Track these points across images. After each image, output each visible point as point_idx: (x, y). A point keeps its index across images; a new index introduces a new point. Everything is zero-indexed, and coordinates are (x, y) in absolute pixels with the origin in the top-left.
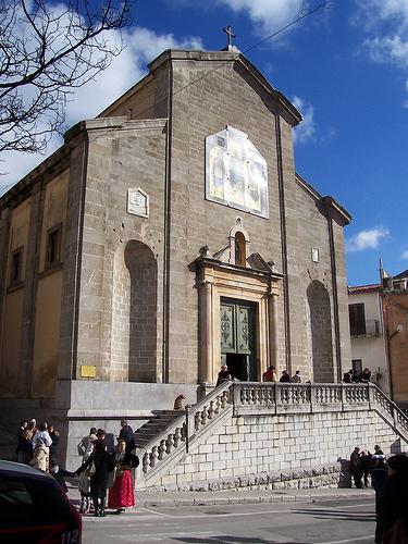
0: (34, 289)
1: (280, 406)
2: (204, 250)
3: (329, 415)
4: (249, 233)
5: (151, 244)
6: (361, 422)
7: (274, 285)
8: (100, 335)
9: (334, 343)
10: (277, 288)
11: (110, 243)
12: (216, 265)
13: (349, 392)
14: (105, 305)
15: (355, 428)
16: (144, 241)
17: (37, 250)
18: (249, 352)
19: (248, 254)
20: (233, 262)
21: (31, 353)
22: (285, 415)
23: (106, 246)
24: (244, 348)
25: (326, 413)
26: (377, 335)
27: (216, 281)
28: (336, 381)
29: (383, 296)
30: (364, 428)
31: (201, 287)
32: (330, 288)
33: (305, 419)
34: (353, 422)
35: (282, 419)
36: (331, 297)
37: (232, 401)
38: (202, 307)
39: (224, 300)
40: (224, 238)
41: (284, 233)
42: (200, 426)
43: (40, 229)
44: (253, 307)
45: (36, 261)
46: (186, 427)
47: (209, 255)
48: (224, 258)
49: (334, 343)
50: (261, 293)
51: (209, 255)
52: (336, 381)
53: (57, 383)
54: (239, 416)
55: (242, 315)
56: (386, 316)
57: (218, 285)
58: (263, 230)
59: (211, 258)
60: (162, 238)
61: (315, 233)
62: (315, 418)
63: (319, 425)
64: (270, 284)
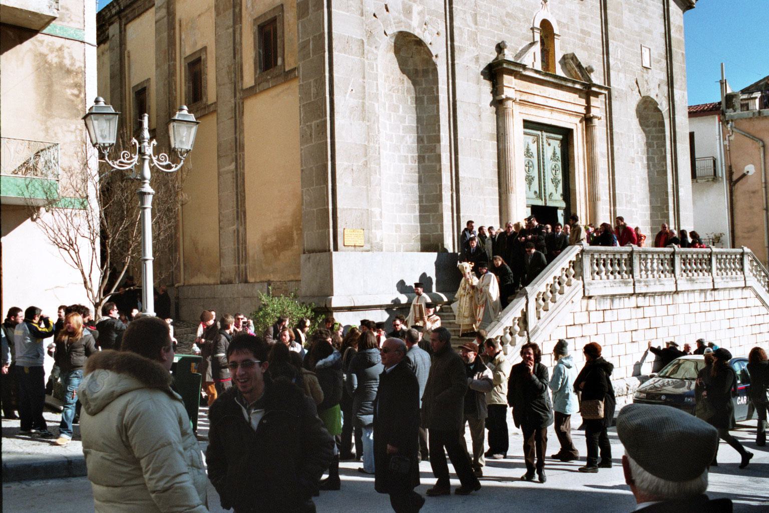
0: (238, 113)
1: (640, 282)
2: (500, 48)
3: (697, 294)
4: (559, 23)
5: (427, 38)
6: (733, 304)
7: (594, 101)
8: (368, 181)
9: (670, 190)
10: (598, 106)
11: (370, 34)
12: (518, 71)
13: (719, 261)
14: (370, 135)
15: (729, 314)
16: (418, 32)
17: (236, 50)
18: (563, 205)
19: (558, 56)
20: (538, 66)
21: (241, 214)
22: (645, 295)
23: (365, 41)
24: (556, 200)
25: (693, 291)
26: (715, 177)
27: (518, 97)
28: (439, 230)
29: (724, 122)
30: (738, 313)
31: (499, 103)
32: (664, 107)
33: (668, 300)
34: (724, 305)
35: (641, 301)
36: (667, 122)
37: (579, 274)
38: (501, 136)
39: (528, 124)
40: (525, 30)
41: (605, 23)
42: (543, 314)
43: (237, 18)
44: (566, 135)
45: (237, 70)
46: (525, 315)
47: (509, 55)
48: (527, 60)
49: (670, 190)
50: (577, 114)
51: (509, 55)
52: (439, 230)
53: (303, 257)
54: (590, 297)
55: (553, 147)
56: (728, 152)
57: (523, 103)
58: (576, 17)
59: (512, 59)
60: (442, 28)
61: (646, 23)
62: (679, 298)
63: (684, 309)
64: (588, 102)
